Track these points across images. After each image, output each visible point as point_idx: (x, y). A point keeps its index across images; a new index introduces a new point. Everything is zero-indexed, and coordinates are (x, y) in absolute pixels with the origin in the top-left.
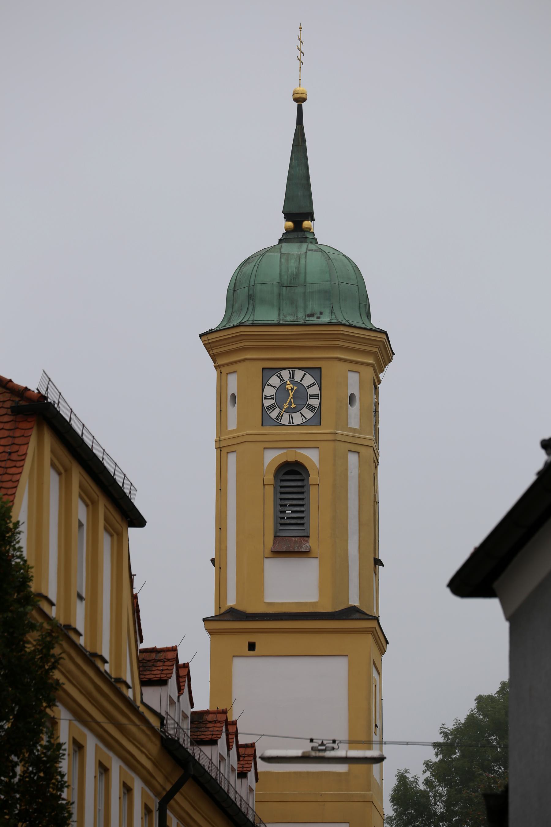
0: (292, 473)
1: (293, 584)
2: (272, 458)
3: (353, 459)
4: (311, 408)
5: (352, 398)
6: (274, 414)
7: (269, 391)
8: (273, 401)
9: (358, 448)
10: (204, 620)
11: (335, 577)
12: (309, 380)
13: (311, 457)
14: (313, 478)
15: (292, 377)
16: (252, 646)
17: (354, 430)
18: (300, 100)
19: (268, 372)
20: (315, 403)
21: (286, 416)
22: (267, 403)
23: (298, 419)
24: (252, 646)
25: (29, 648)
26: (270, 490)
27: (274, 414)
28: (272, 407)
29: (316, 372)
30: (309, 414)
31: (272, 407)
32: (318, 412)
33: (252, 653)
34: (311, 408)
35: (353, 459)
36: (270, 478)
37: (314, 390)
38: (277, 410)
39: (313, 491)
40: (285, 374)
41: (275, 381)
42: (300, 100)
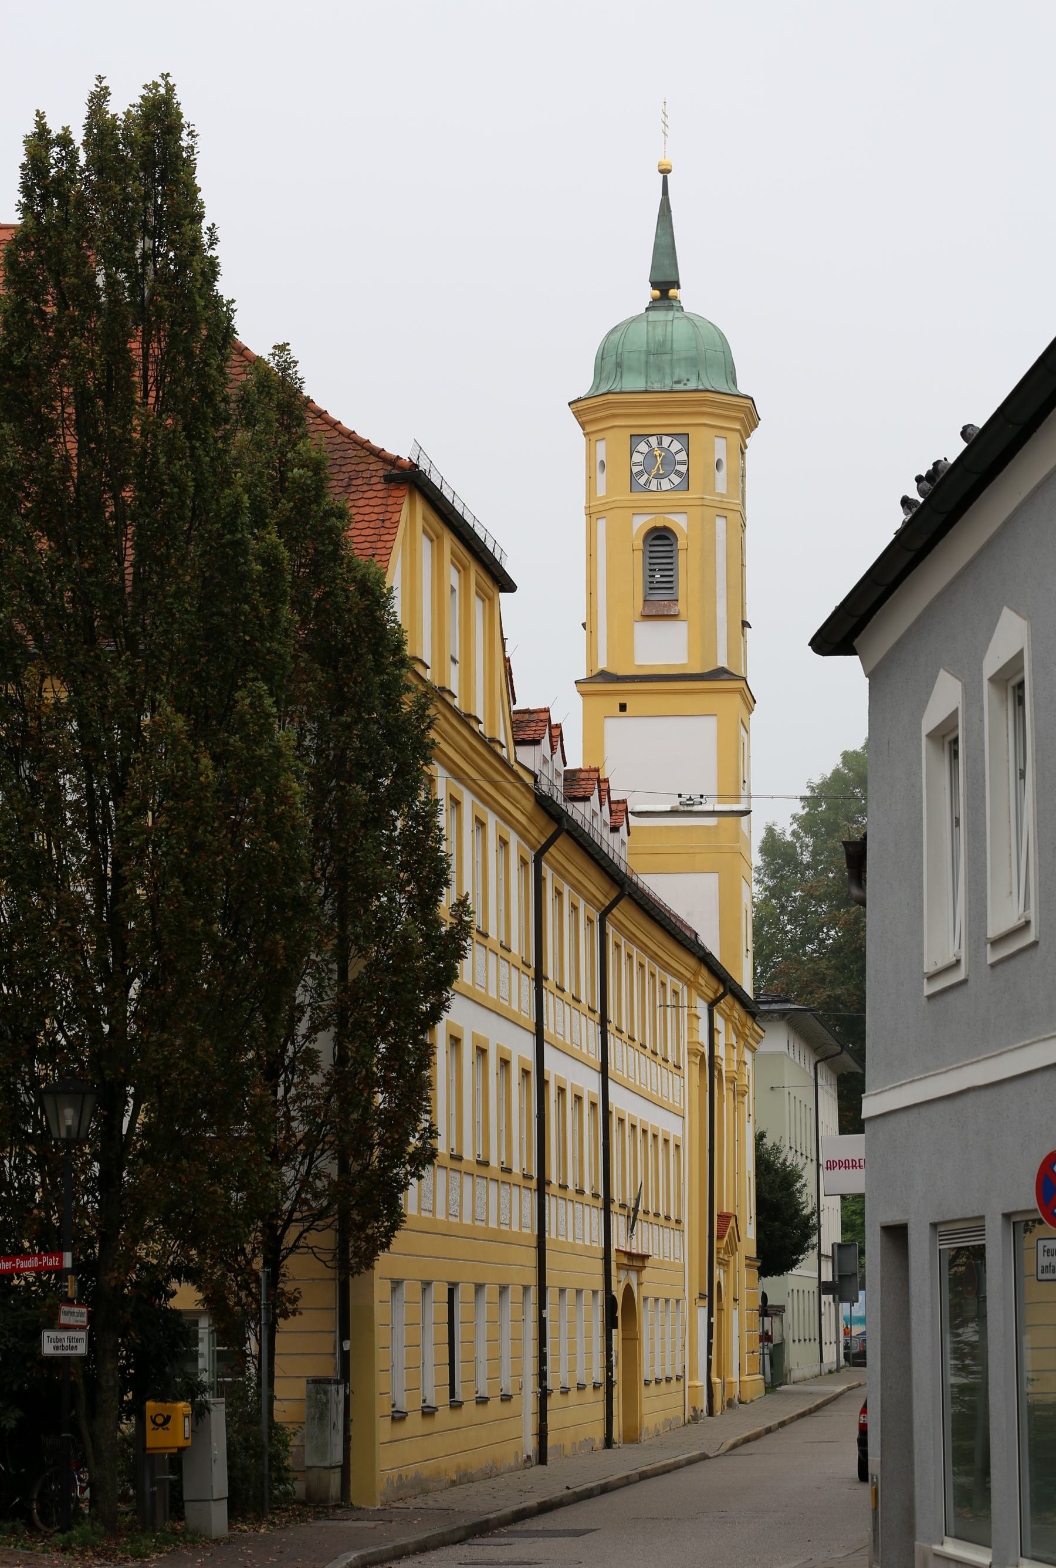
0: (661, 537)
1: (662, 647)
2: (641, 524)
4: (678, 473)
6: (642, 481)
7: (637, 458)
11: (704, 638)
12: (676, 446)
13: (679, 522)
14: (681, 543)
15: (660, 443)
16: (623, 707)
17: (722, 495)
18: (665, 172)
20: (683, 468)
21: (654, 482)
22: (635, 469)
23: (666, 485)
24: (623, 707)
27: (642, 481)
28: (640, 474)
30: (676, 480)
31: (640, 474)
32: (686, 477)
33: (623, 713)
34: (678, 473)
35: (720, 523)
36: (639, 543)
37: (682, 456)
38: (646, 476)
39: (681, 557)
40: (653, 441)
41: (643, 447)
42: (665, 172)
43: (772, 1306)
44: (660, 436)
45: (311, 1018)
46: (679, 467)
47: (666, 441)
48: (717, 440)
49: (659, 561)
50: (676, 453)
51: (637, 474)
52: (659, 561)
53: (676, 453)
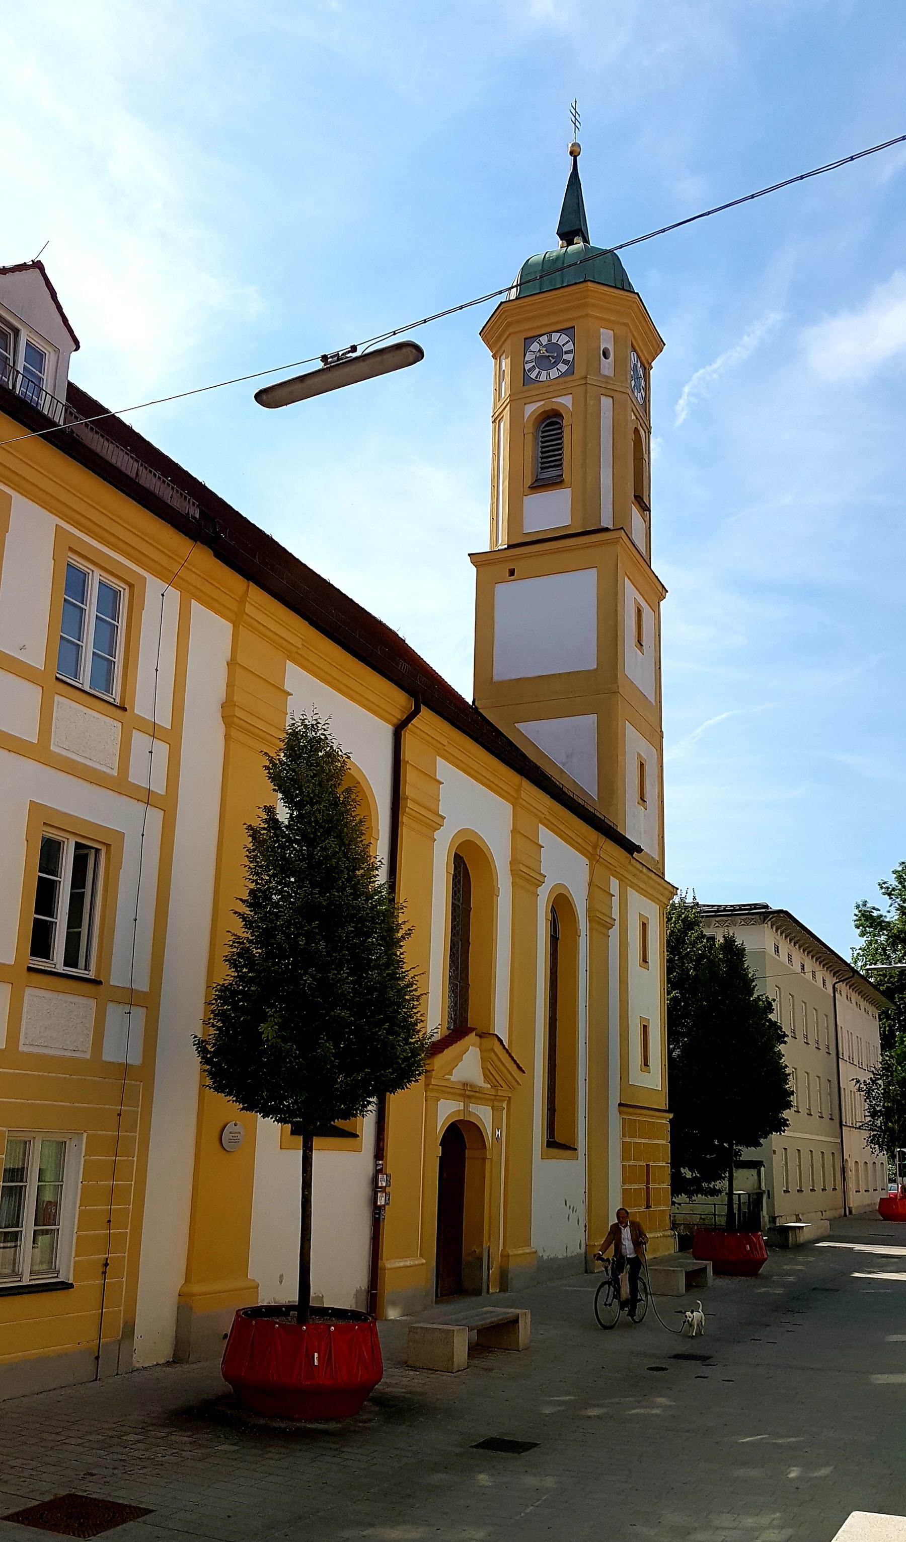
0: (551, 424)
1: (552, 511)
2: (531, 409)
3: (606, 403)
4: (566, 362)
5: (606, 354)
8: (537, 370)
9: (612, 394)
10: (469, 555)
11: (587, 501)
12: (564, 338)
13: (566, 401)
16: (512, 573)
18: (574, 154)
19: (529, 340)
20: (569, 357)
22: (528, 367)
23: (554, 374)
24: (512, 573)
25: (628, 1266)
26: (529, 438)
27: (533, 376)
29: (569, 331)
30: (563, 368)
32: (571, 364)
34: (566, 362)
36: (530, 429)
40: (544, 340)
42: (574, 154)
43: (491, 547)
44: (549, 334)
45: (559, 1411)
46: (565, 357)
47: (555, 337)
48: (603, 398)
49: (553, 437)
50: (566, 353)
51: (529, 370)
52: (553, 437)
53: (566, 353)
